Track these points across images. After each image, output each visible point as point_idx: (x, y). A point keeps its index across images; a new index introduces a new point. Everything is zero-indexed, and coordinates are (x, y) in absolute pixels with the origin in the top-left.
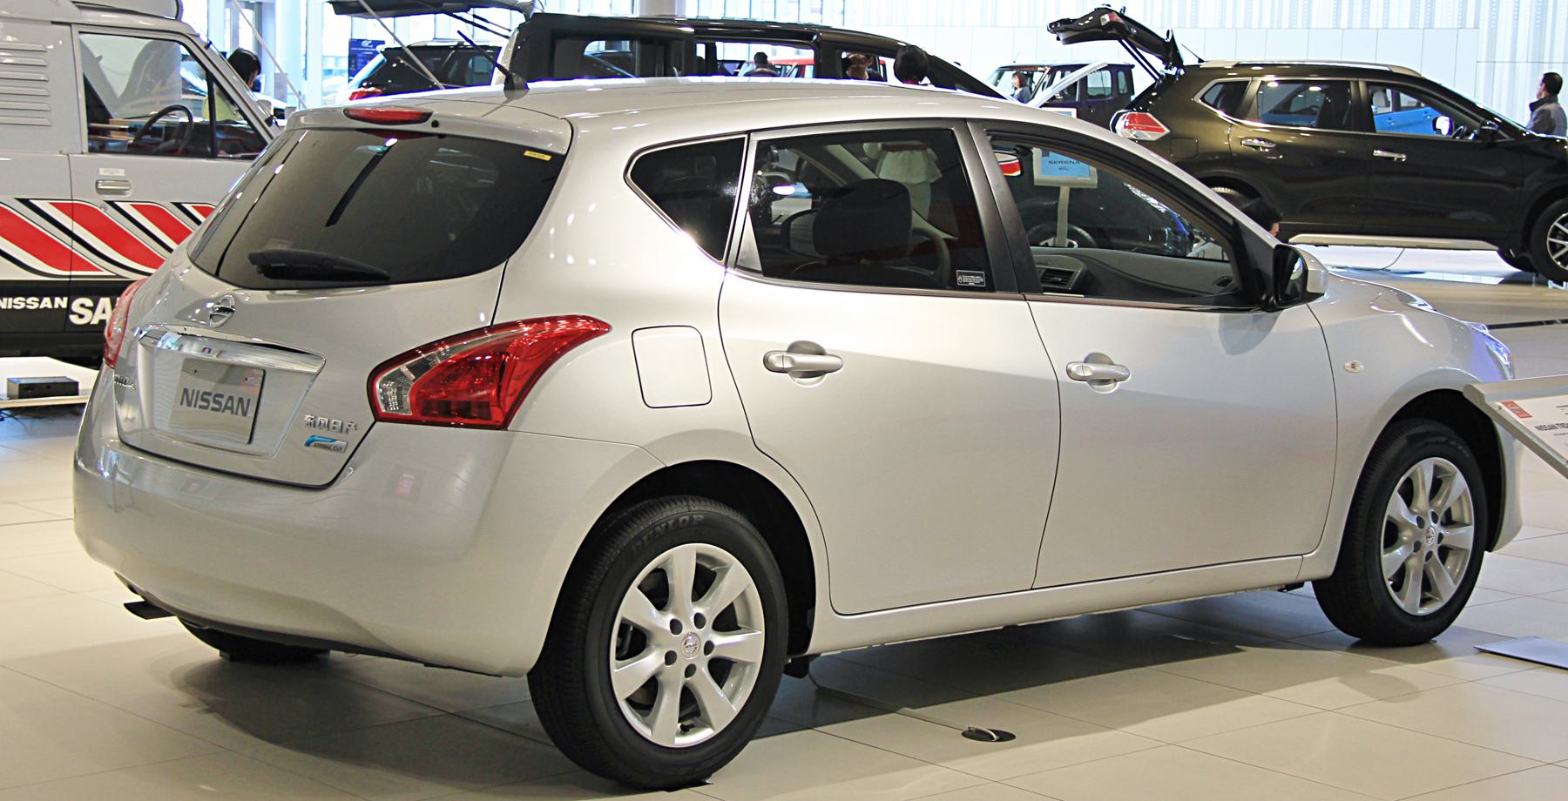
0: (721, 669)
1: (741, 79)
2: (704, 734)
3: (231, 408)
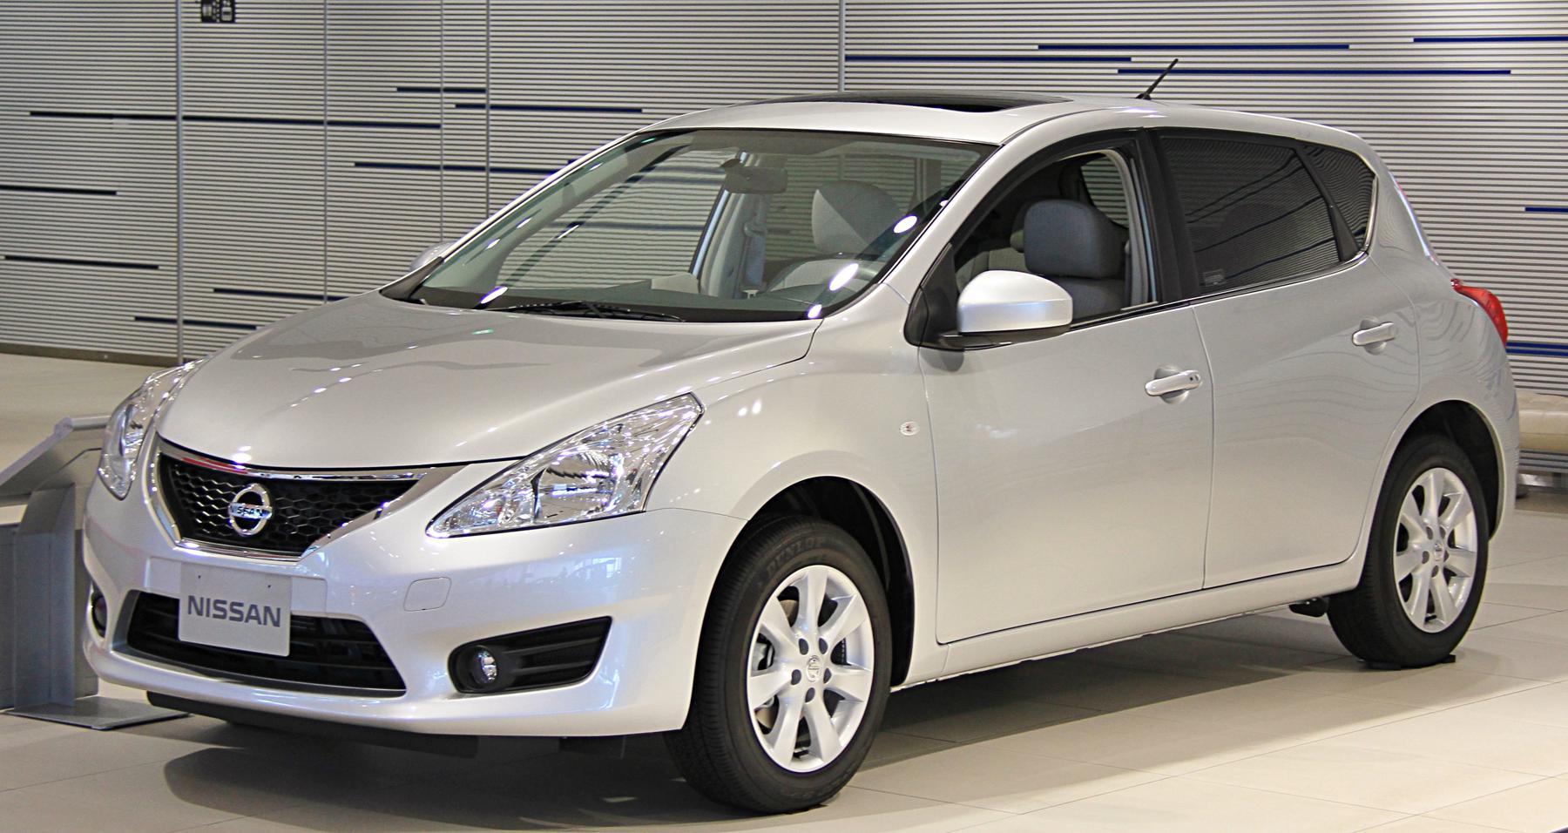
0: (832, 700)
1: (1013, 135)
2: (814, 764)
3: (257, 618)
